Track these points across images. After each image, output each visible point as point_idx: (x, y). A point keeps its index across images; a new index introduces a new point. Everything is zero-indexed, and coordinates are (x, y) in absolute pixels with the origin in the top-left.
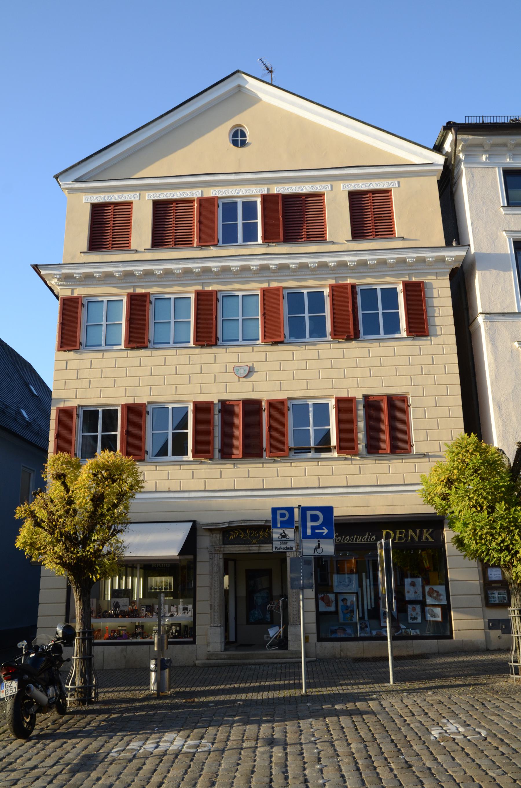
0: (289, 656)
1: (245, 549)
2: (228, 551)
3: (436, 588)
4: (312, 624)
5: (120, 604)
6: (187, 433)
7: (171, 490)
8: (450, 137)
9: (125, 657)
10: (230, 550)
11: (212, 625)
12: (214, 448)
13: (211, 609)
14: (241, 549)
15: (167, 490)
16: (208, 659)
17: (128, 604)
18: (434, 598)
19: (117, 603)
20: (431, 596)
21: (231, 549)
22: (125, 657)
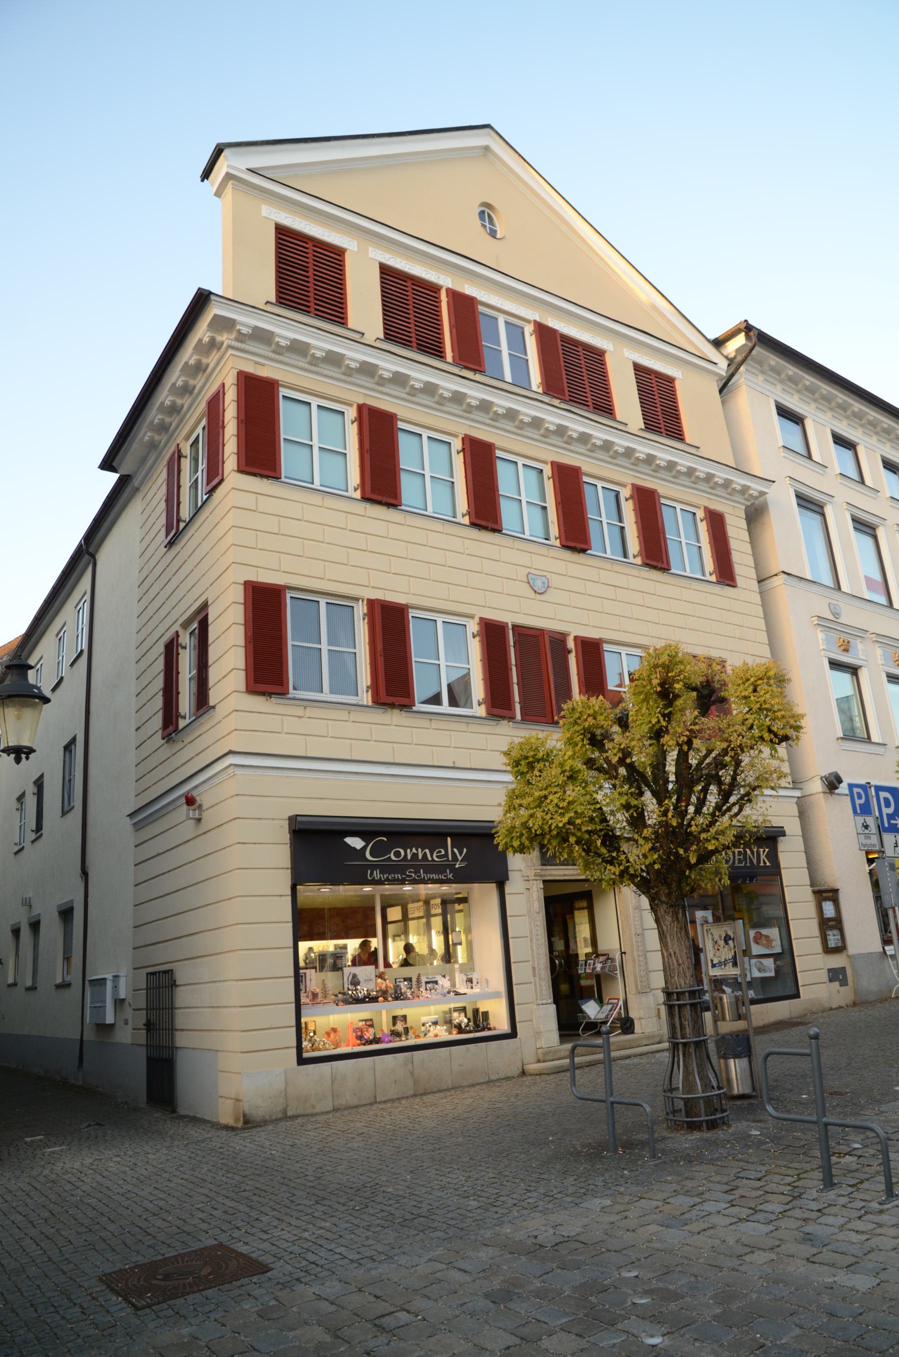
0: (645, 1042)
1: (554, 872)
2: (550, 875)
3: (764, 932)
4: (290, 1050)
5: (359, 977)
6: (329, 645)
7: (457, 765)
8: (740, 340)
9: (412, 1073)
10: (553, 875)
11: (540, 1002)
12: (514, 702)
13: (534, 975)
14: (567, 872)
15: (452, 765)
16: (539, 1061)
17: (373, 977)
18: (763, 945)
19: (355, 976)
20: (757, 943)
21: (554, 872)
22: (412, 1073)
